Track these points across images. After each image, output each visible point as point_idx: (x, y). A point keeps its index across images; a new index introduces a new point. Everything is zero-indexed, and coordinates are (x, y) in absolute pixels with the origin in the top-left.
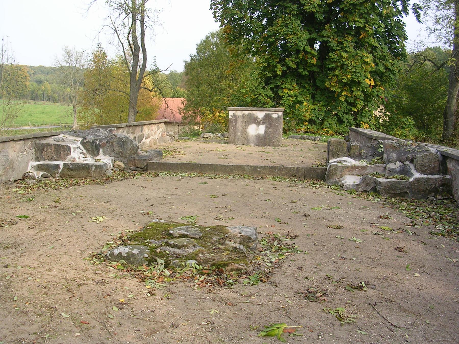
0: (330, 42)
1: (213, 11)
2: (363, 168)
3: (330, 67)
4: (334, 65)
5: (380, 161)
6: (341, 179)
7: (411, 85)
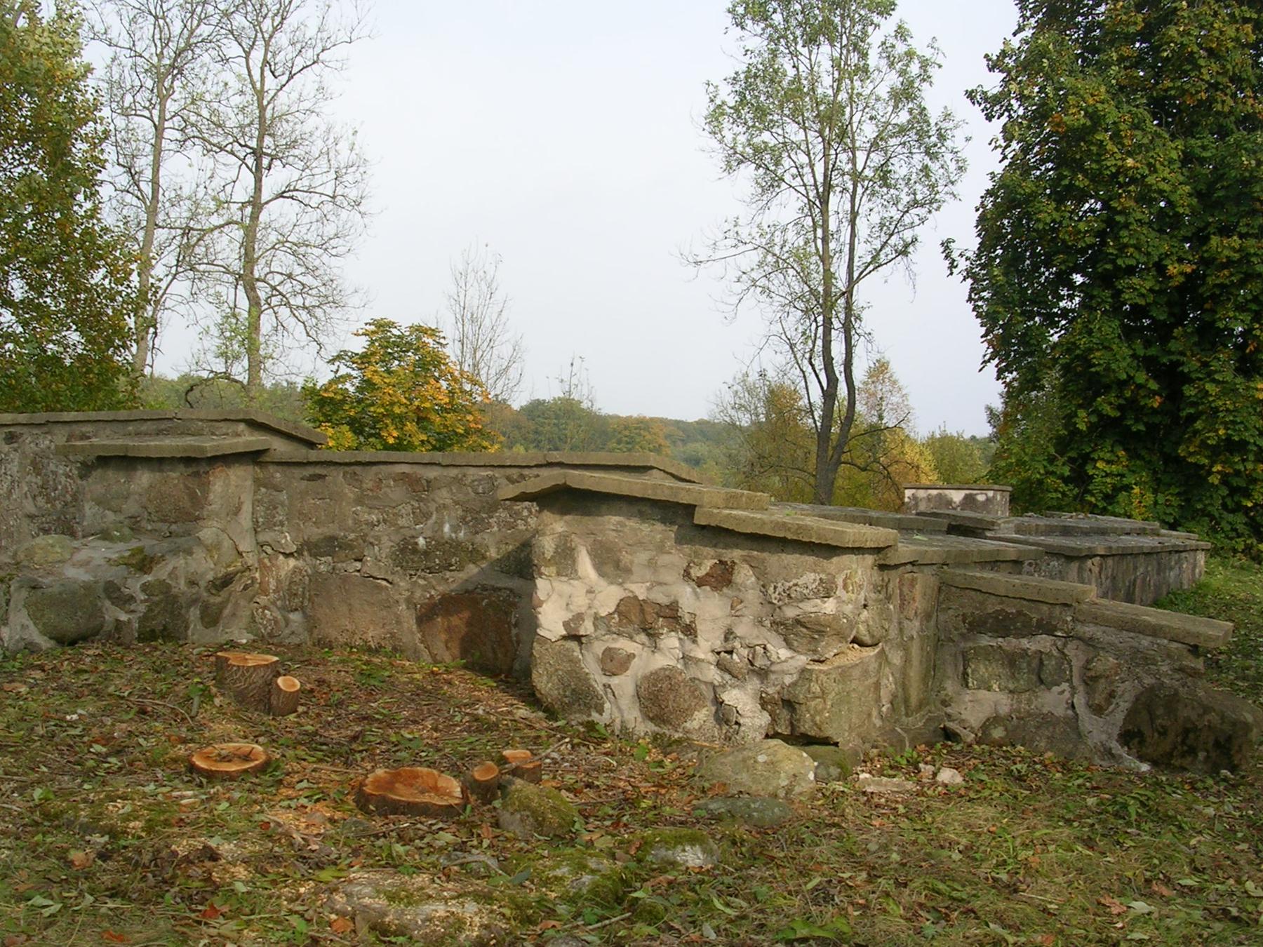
0: (1183, 364)
4: (1192, 411)
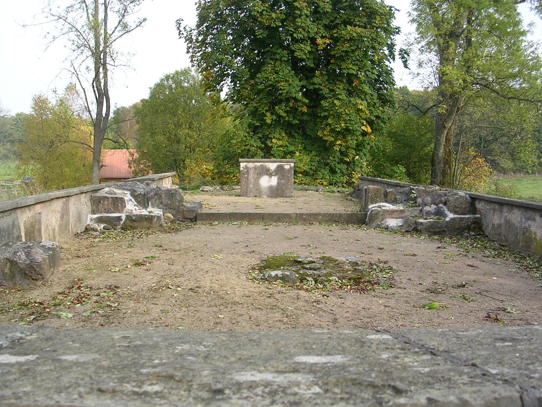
0: (321, 90)
1: (190, 54)
2: (402, 211)
3: (322, 115)
4: (326, 114)
5: (414, 205)
6: (383, 222)
7: (395, 132)
